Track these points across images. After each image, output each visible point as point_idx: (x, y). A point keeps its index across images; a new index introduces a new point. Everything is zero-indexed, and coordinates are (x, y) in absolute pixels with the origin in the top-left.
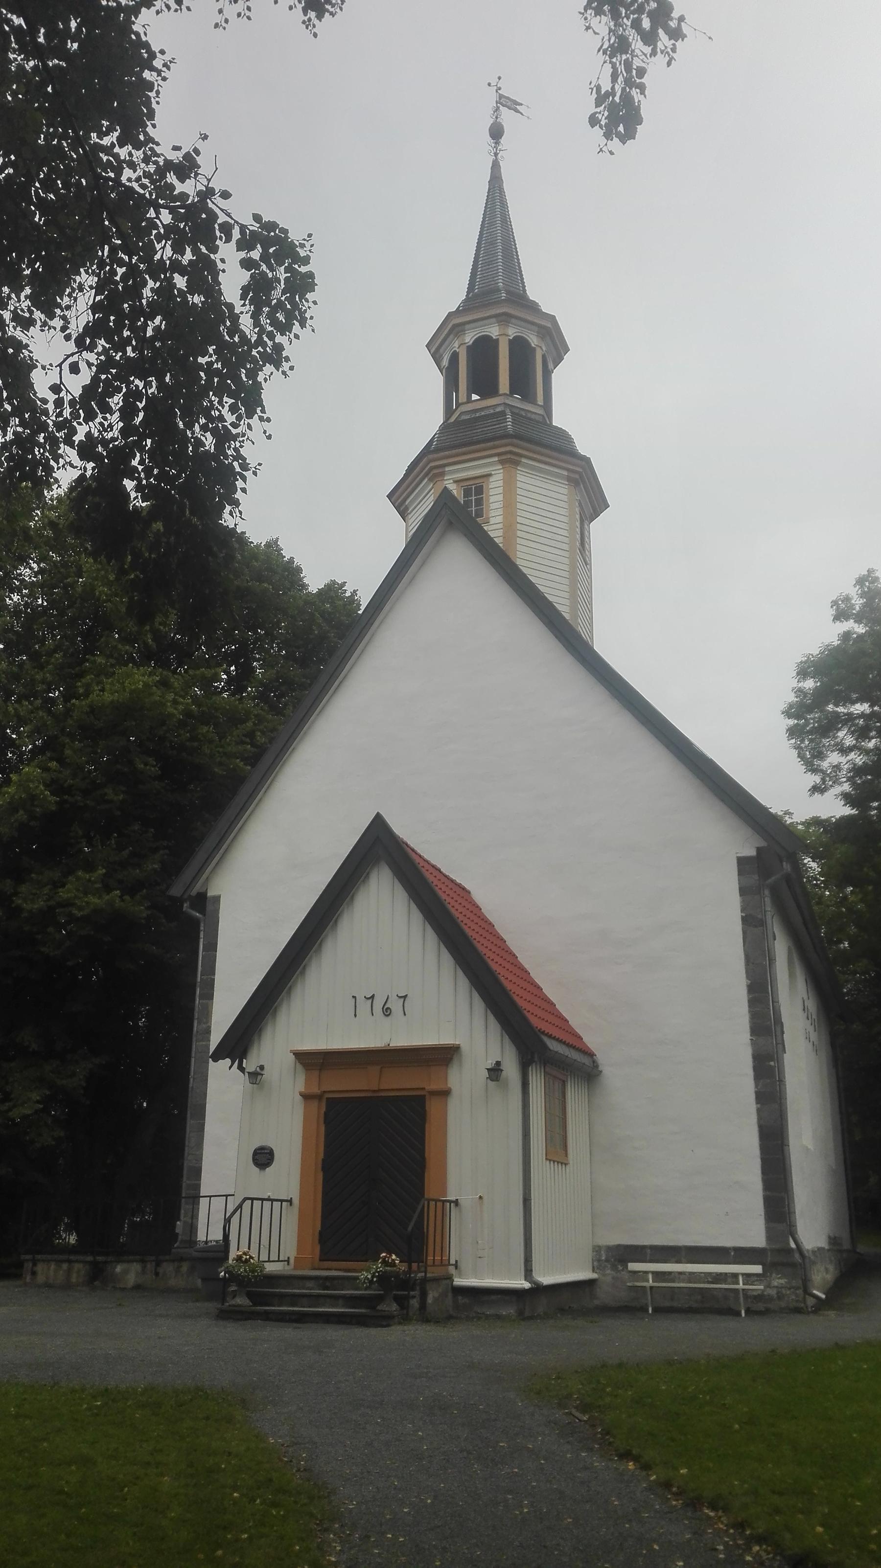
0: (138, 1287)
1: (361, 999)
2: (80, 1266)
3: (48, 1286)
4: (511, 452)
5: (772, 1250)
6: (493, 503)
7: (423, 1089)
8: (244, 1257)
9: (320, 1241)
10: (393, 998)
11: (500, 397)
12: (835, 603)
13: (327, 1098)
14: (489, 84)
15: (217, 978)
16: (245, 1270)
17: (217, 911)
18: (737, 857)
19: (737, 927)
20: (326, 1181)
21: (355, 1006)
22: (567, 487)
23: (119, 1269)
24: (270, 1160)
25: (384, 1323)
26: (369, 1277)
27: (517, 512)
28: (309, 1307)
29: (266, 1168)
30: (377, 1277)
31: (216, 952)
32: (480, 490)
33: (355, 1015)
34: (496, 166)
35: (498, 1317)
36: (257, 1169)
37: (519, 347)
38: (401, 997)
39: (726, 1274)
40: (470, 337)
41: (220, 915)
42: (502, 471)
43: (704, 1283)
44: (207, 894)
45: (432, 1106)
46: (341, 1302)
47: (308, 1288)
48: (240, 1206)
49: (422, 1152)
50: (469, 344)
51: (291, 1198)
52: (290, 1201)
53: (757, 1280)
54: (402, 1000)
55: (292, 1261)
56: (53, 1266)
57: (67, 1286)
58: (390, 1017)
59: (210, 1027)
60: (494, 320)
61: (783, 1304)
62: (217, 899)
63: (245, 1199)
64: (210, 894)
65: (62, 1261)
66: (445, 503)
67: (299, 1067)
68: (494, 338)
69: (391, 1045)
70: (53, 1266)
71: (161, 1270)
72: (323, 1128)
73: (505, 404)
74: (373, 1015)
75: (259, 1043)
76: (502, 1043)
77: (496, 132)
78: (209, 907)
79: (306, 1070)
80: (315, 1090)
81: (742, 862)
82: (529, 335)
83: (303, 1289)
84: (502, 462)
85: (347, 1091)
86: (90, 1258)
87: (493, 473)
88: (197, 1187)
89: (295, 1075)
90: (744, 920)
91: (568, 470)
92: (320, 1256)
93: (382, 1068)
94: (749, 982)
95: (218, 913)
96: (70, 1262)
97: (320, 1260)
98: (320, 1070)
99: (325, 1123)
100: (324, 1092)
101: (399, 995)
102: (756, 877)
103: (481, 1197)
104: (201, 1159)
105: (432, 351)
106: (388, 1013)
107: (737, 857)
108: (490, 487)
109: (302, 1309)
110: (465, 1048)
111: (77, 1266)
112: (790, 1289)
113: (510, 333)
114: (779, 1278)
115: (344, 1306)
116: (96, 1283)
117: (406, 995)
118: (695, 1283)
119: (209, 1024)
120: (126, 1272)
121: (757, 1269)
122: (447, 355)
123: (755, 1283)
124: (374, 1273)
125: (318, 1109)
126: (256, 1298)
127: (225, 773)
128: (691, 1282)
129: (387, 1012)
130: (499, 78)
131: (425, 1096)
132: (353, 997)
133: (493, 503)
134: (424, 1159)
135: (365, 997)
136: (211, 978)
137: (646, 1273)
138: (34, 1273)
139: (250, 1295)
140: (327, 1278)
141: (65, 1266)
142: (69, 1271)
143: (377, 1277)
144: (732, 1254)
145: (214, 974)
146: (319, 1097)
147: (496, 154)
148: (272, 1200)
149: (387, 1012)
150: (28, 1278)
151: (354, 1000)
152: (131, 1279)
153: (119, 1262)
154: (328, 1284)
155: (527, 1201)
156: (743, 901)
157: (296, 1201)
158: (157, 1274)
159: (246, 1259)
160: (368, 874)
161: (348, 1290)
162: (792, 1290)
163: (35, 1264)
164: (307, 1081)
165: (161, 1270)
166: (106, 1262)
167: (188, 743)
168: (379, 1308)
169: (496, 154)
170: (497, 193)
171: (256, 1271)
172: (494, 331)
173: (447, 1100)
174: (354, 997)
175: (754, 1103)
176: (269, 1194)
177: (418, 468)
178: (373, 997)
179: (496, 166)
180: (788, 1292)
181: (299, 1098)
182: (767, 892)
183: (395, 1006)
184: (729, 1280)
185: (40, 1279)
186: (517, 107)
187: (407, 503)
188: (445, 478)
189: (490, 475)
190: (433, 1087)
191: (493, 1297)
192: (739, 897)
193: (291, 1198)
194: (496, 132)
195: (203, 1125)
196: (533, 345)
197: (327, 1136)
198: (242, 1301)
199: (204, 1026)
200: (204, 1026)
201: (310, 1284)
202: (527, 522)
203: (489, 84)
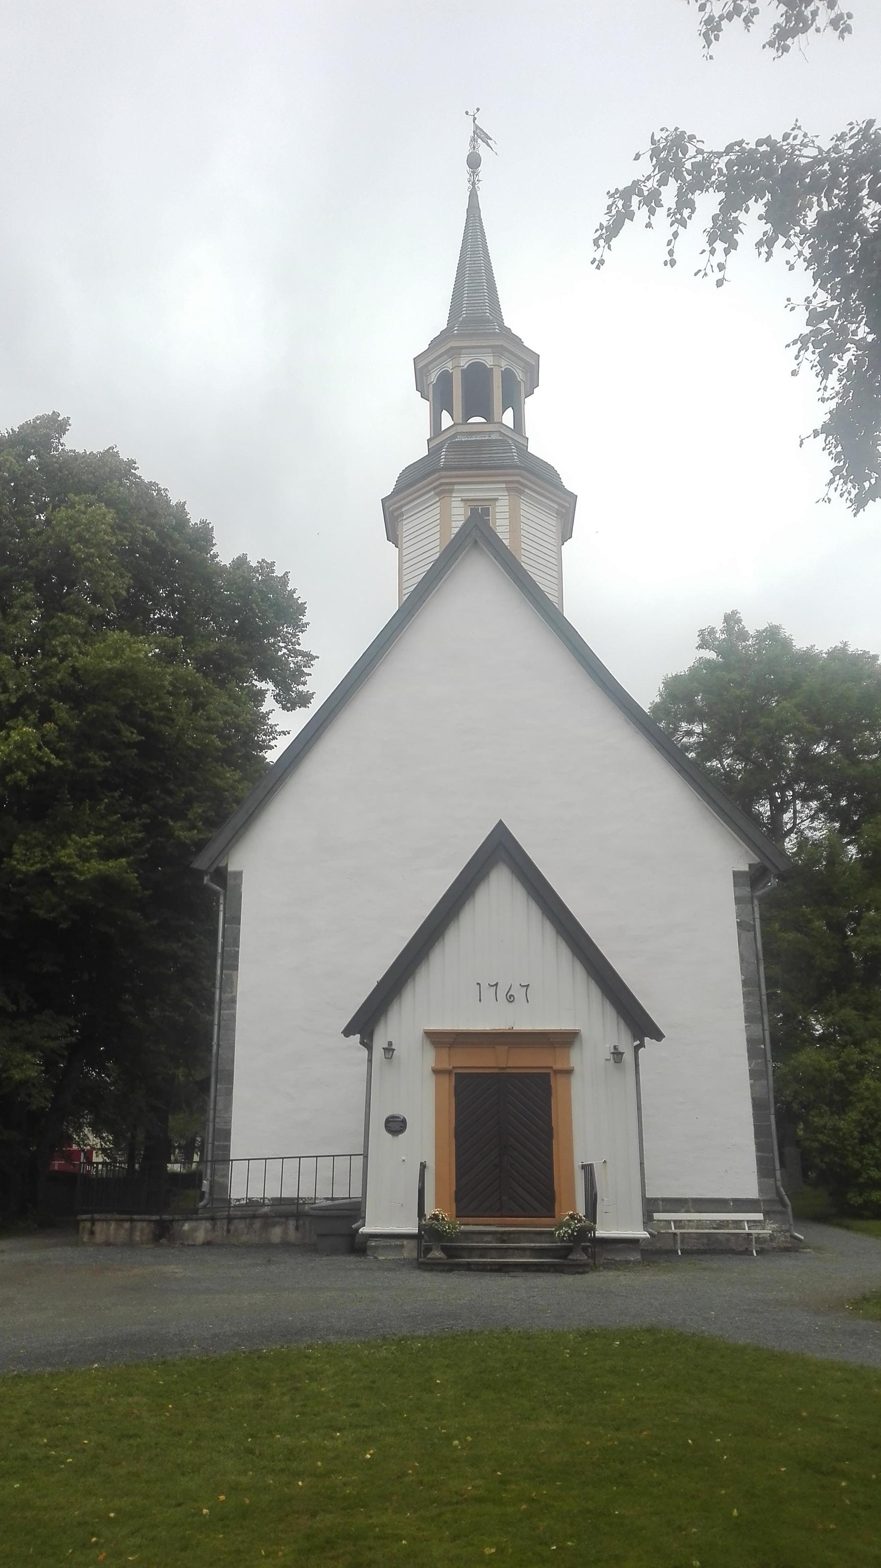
0: (208, 1244)
1: (484, 986)
2: (145, 1224)
3: (107, 1244)
4: (518, 482)
5: (764, 1201)
6: (499, 526)
7: (551, 1068)
10: (516, 987)
11: (494, 425)
12: (702, 633)
13: (456, 1074)
14: (467, 113)
16: (449, 1228)
17: (239, 886)
18: (733, 871)
19: (734, 930)
22: (555, 519)
23: (186, 1227)
25: (581, 1271)
26: (570, 1231)
27: (521, 538)
28: (499, 1258)
29: (398, 1135)
31: (240, 924)
32: (486, 511)
34: (473, 197)
35: (628, 1262)
36: (390, 1136)
37: (508, 377)
39: (728, 1221)
40: (465, 362)
41: (242, 890)
42: (507, 498)
43: (710, 1229)
44: (227, 869)
45: (557, 1083)
46: (528, 1252)
47: (486, 1242)
50: (463, 368)
53: (753, 1226)
56: (113, 1226)
57: (131, 1244)
58: (513, 1003)
60: (490, 350)
61: (774, 1245)
62: (239, 875)
64: (231, 868)
65: (123, 1220)
66: (476, 525)
68: (488, 367)
69: (514, 1028)
70: (113, 1226)
71: (232, 1228)
72: (453, 1100)
73: (499, 431)
74: (497, 1000)
75: (386, 1022)
76: (618, 1031)
77: (474, 162)
78: (230, 882)
79: (435, 1047)
80: (446, 1066)
81: (736, 875)
82: (518, 370)
83: (481, 1243)
84: (508, 489)
85: (472, 1067)
86: (155, 1218)
87: (500, 498)
88: (227, 1148)
89: (423, 1053)
90: (739, 925)
91: (558, 504)
92: (456, 1214)
94: (743, 977)
96: (132, 1221)
98: (449, 1047)
100: (454, 1068)
101: (491, 984)
102: (749, 889)
103: (605, 1162)
105: (419, 366)
107: (733, 871)
108: (496, 511)
109: (492, 1260)
110: (584, 1033)
111: (139, 1225)
112: (780, 1232)
113: (503, 366)
114: (771, 1224)
115: (531, 1257)
116: (163, 1241)
117: (529, 985)
118: (702, 1229)
119: (234, 994)
120: (194, 1230)
121: (759, 1216)
122: (436, 372)
123: (752, 1228)
125: (448, 1083)
126: (450, 1252)
127: (199, 747)
128: (698, 1229)
129: (510, 999)
130: (478, 110)
131: (549, 1073)
132: (478, 984)
133: (499, 526)
134: (551, 1129)
135: (489, 984)
136: (235, 950)
137: (669, 1222)
138: (92, 1233)
139: (444, 1249)
140: (503, 1233)
141: (127, 1225)
142: (132, 1230)
144: (731, 1204)
145: (239, 947)
146: (449, 1072)
147: (474, 184)
149: (510, 999)
150: (86, 1238)
151: (478, 986)
152: (201, 1236)
153: (187, 1220)
155: (642, 1164)
156: (738, 909)
158: (228, 1231)
161: (524, 1243)
162: (782, 1233)
163: (93, 1225)
164: (437, 1058)
165: (232, 1228)
166: (172, 1221)
167: (154, 712)
168: (570, 1257)
169: (474, 184)
170: (477, 222)
172: (489, 361)
173: (570, 1078)
175: (748, 1079)
177: (426, 481)
178: (496, 984)
179: (473, 197)
180: (779, 1235)
182: (756, 902)
183: (517, 992)
184: (731, 1225)
185: (99, 1237)
186: (488, 140)
187: (403, 510)
188: (453, 495)
189: (497, 500)
190: (558, 1066)
191: (620, 1246)
192: (734, 905)
194: (474, 162)
196: (519, 379)
198: (437, 1254)
199: (230, 995)
201: (488, 1238)
202: (528, 548)
203: (467, 113)
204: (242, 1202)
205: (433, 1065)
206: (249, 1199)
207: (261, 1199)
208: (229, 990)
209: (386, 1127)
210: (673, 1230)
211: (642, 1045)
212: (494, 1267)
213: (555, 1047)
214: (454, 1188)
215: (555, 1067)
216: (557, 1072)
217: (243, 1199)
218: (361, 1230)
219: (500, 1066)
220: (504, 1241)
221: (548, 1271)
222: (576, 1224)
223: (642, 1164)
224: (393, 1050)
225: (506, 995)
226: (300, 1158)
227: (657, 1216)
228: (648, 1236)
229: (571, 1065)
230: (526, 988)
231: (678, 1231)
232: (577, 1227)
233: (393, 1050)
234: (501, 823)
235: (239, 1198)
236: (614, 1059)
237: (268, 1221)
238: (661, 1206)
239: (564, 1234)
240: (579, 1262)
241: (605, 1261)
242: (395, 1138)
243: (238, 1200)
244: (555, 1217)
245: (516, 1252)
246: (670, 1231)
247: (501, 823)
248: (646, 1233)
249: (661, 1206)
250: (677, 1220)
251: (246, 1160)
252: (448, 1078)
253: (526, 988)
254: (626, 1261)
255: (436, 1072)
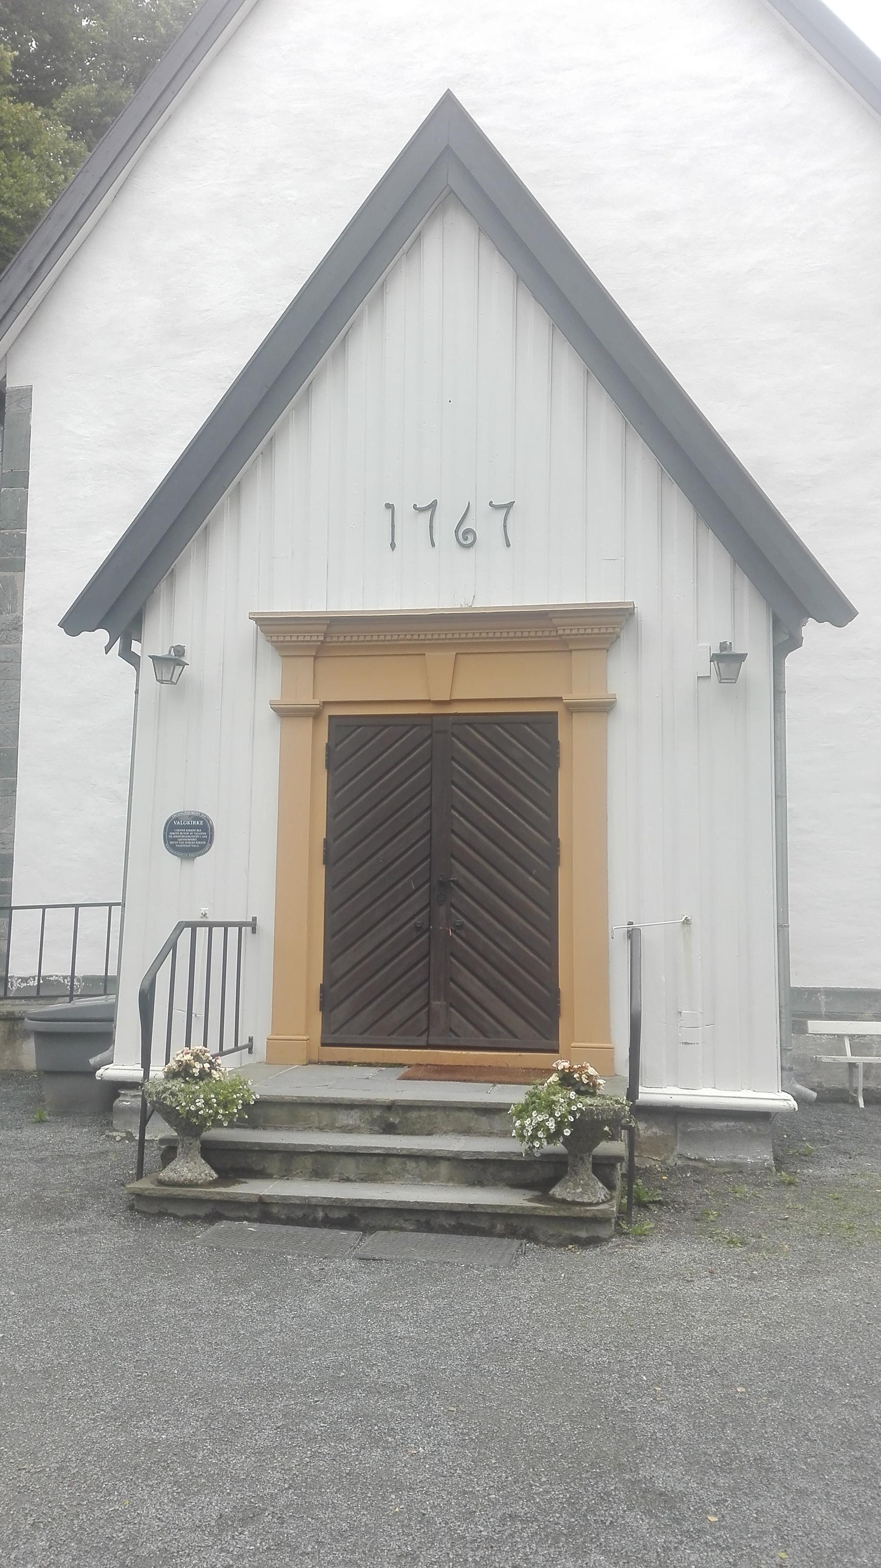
1: (404, 511)
8: (198, 1065)
9: (323, 1006)
13: (330, 717)
15: (30, 533)
16: (207, 1103)
20: (332, 885)
21: (393, 526)
24: (206, 840)
29: (193, 858)
30: (571, 1125)
33: (393, 546)
38: (498, 507)
41: (32, 423)
46: (444, 1168)
48: (172, 946)
49: (550, 830)
51: (254, 919)
52: (253, 925)
54: (502, 514)
55: (260, 1046)
59: (20, 619)
62: (26, 394)
63: (180, 927)
67: (267, 652)
74: (433, 545)
80: (307, 699)
93: (457, 654)
95: (29, 418)
97: (323, 1045)
98: (316, 658)
99: (328, 766)
103: (687, 922)
104: (12, 841)
106: (468, 542)
124: (563, 1116)
132: (389, 506)
136: (18, 534)
137: (840, 1037)
143: (571, 1125)
146: (315, 714)
148: (211, 925)
149: (466, 539)
154: (393, 1119)
157: (267, 924)
159: (202, 1070)
160: (419, 236)
168: (557, 1191)
171: (233, 1102)
174: (389, 506)
176: (204, 909)
178: (433, 506)
181: (266, 714)
190: (578, 694)
191: (718, 1125)
193: (254, 919)
195: (15, 784)
197: (332, 792)
199: (10, 617)
200: (10, 617)
204: (31, 984)
205: (277, 697)
206: (44, 978)
207: (65, 977)
208: (9, 607)
209: (167, 840)
210: (849, 1057)
211: (794, 642)
212: (336, 1215)
213: (571, 651)
214: (318, 979)
215: (567, 697)
216: (575, 709)
217: (34, 978)
218: (99, 1073)
219: (434, 698)
220: (389, 1129)
221: (487, 1233)
222: (570, 1102)
223: (782, 927)
224: (184, 664)
225: (456, 532)
226: (44, 908)
227: (815, 1026)
228: (794, 1104)
229: (610, 692)
230: (504, 511)
231: (859, 1060)
232: (572, 1113)
233: (184, 664)
234: (448, 101)
235: (27, 976)
236: (719, 674)
237: (16, 1028)
238: (823, 1004)
239: (536, 1129)
240: (577, 1211)
241: (679, 1163)
242: (187, 865)
243: (25, 980)
244: (558, 1053)
245: (411, 1165)
246: (841, 1059)
247: (448, 101)
248: (790, 1097)
249: (823, 1004)
250: (854, 1035)
251: (72, 906)
252: (311, 724)
253: (504, 511)
254: (734, 1164)
255: (284, 713)
